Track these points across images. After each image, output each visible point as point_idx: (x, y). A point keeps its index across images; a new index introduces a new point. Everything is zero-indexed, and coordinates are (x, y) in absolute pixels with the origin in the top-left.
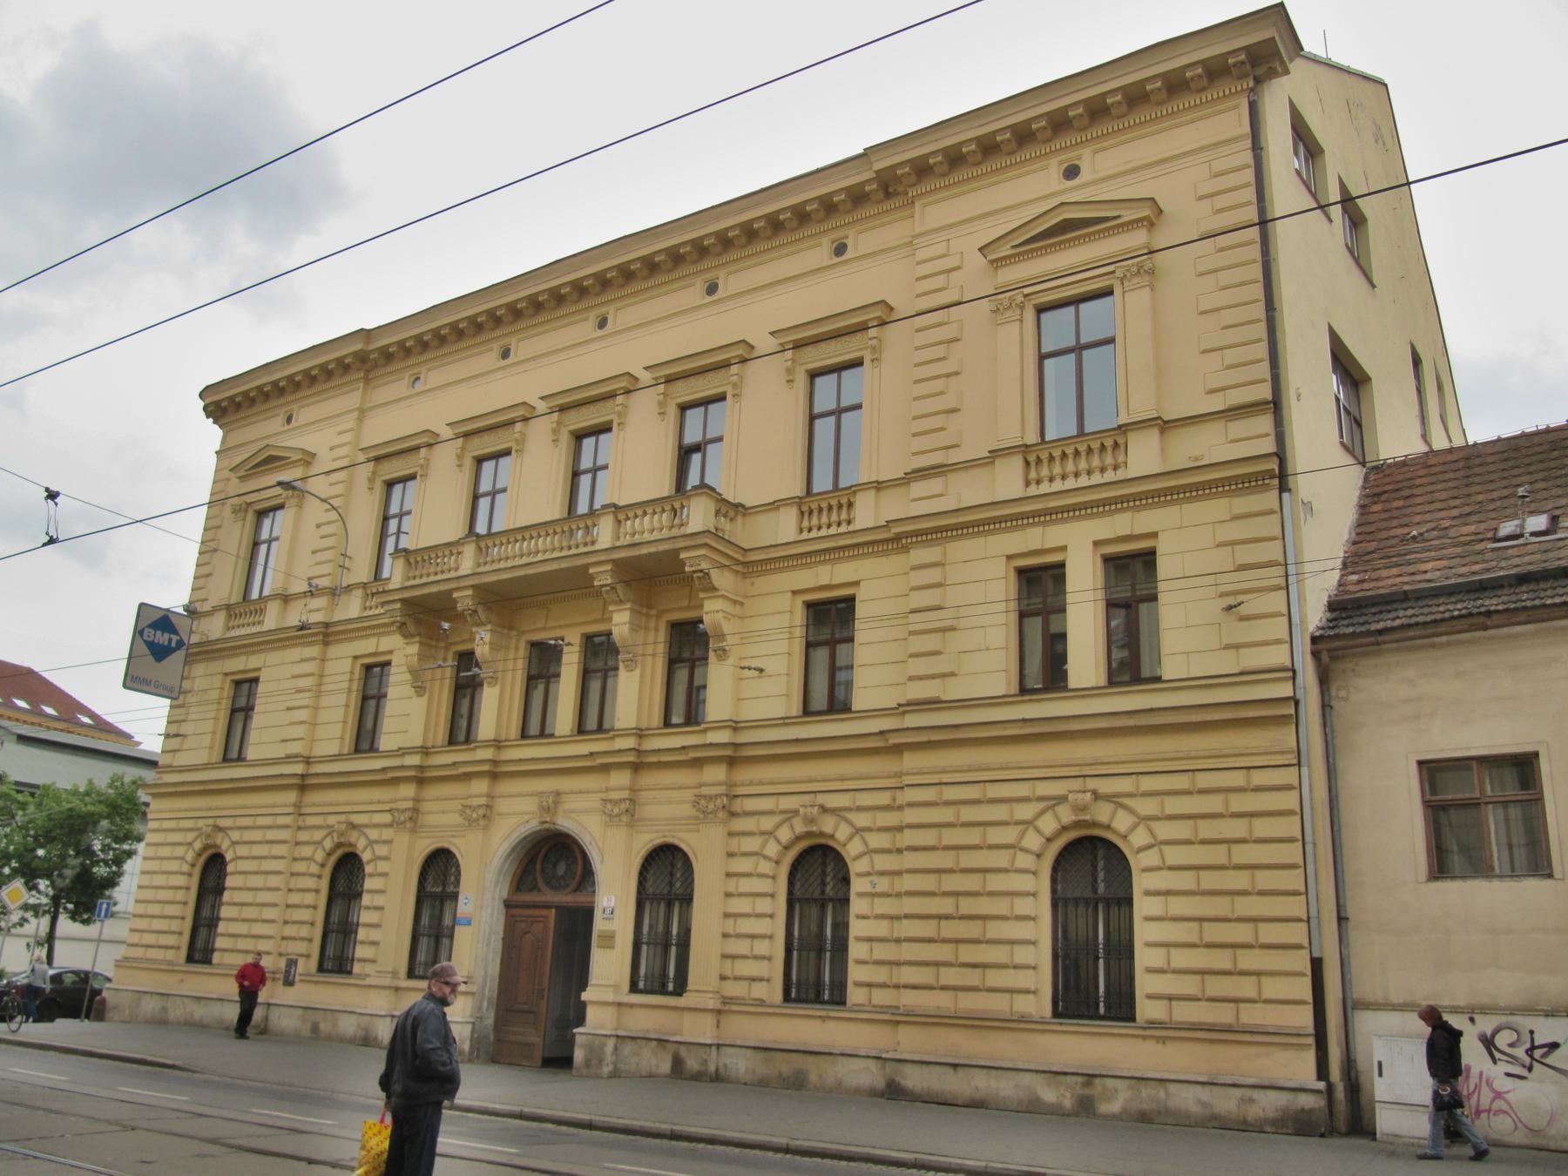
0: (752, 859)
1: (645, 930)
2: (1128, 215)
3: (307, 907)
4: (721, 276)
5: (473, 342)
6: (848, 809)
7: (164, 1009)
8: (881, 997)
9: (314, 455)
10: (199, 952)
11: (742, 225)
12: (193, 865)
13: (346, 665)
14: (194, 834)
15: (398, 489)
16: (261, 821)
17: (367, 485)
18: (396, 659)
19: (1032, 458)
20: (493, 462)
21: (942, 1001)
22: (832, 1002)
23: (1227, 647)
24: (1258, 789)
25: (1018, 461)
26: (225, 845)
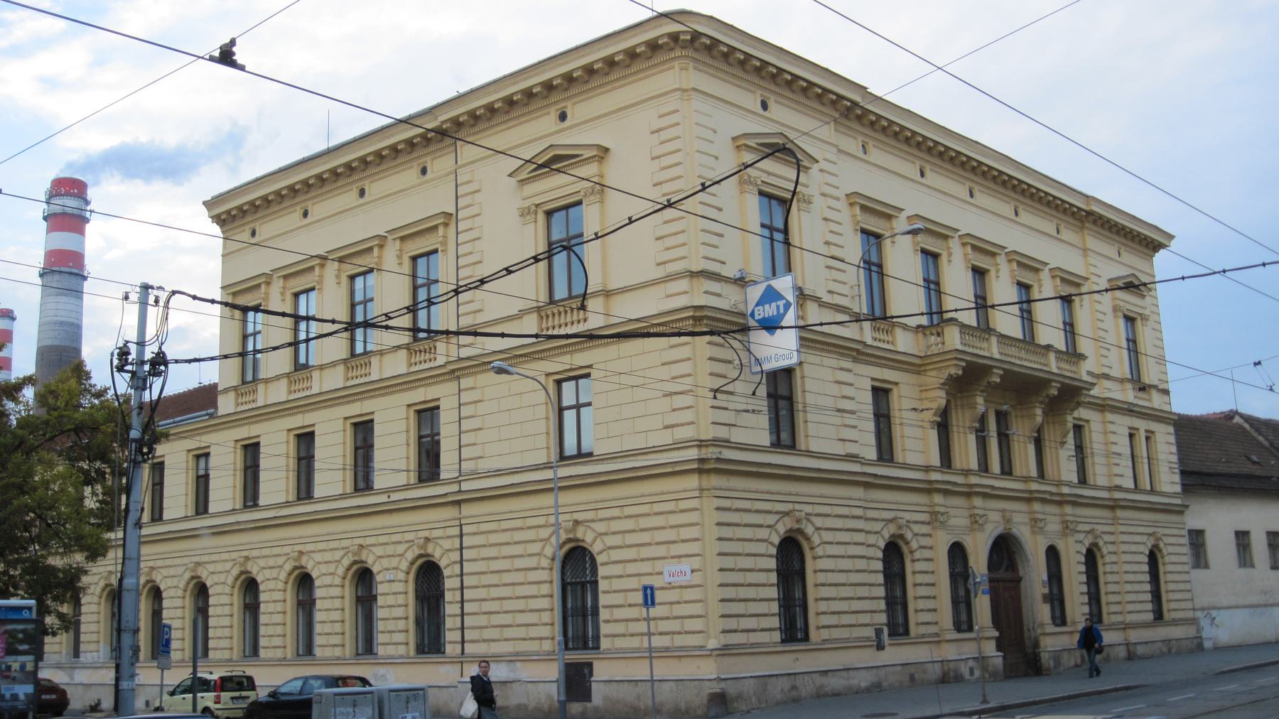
1: (569, 605)
2: (587, 154)
4: (257, 226)
5: (392, 164)
6: (593, 521)
7: (794, 688)
9: (607, 150)
11: (604, 60)
12: (408, 573)
14: (283, 559)
16: (484, 527)
17: (280, 297)
19: (543, 314)
21: (844, 633)
22: (593, 649)
23: (666, 427)
26: (370, 560)
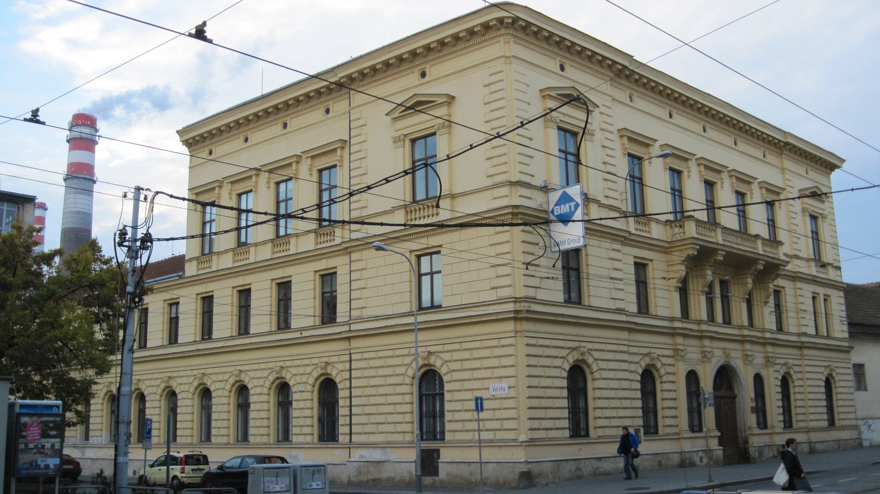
0: (402, 377)
2: (440, 100)
3: (407, 403)
4: (288, 120)
7: (578, 469)
8: (804, 424)
9: (453, 98)
10: (579, 428)
12: (313, 386)
13: (160, 305)
14: (193, 378)
15: (244, 197)
17: (266, 185)
18: (339, 271)
19: (408, 210)
20: (328, 171)
22: (440, 440)
24: (503, 346)
25: (403, 211)
